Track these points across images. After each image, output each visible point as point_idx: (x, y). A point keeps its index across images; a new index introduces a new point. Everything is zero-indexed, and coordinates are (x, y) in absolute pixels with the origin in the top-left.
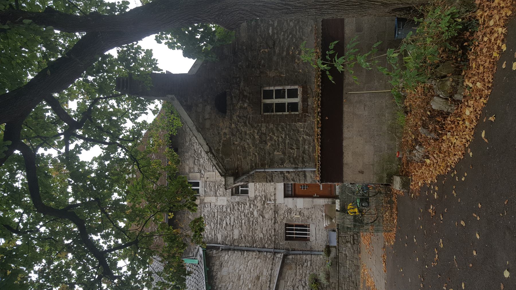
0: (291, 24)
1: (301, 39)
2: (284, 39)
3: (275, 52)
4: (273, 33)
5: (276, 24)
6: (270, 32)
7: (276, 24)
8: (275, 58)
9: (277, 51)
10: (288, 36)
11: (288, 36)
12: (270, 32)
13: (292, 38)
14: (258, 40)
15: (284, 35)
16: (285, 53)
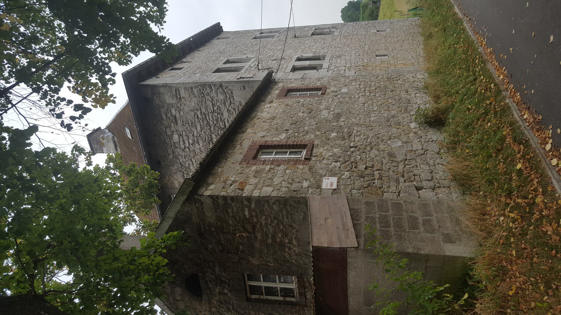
0: (275, 207)
2: (266, 224)
3: (256, 237)
5: (253, 206)
6: (247, 213)
7: (253, 206)
8: (257, 245)
9: (259, 236)
10: (272, 222)
11: (272, 222)
12: (247, 213)
14: (231, 222)
15: (266, 219)
16: (270, 241)
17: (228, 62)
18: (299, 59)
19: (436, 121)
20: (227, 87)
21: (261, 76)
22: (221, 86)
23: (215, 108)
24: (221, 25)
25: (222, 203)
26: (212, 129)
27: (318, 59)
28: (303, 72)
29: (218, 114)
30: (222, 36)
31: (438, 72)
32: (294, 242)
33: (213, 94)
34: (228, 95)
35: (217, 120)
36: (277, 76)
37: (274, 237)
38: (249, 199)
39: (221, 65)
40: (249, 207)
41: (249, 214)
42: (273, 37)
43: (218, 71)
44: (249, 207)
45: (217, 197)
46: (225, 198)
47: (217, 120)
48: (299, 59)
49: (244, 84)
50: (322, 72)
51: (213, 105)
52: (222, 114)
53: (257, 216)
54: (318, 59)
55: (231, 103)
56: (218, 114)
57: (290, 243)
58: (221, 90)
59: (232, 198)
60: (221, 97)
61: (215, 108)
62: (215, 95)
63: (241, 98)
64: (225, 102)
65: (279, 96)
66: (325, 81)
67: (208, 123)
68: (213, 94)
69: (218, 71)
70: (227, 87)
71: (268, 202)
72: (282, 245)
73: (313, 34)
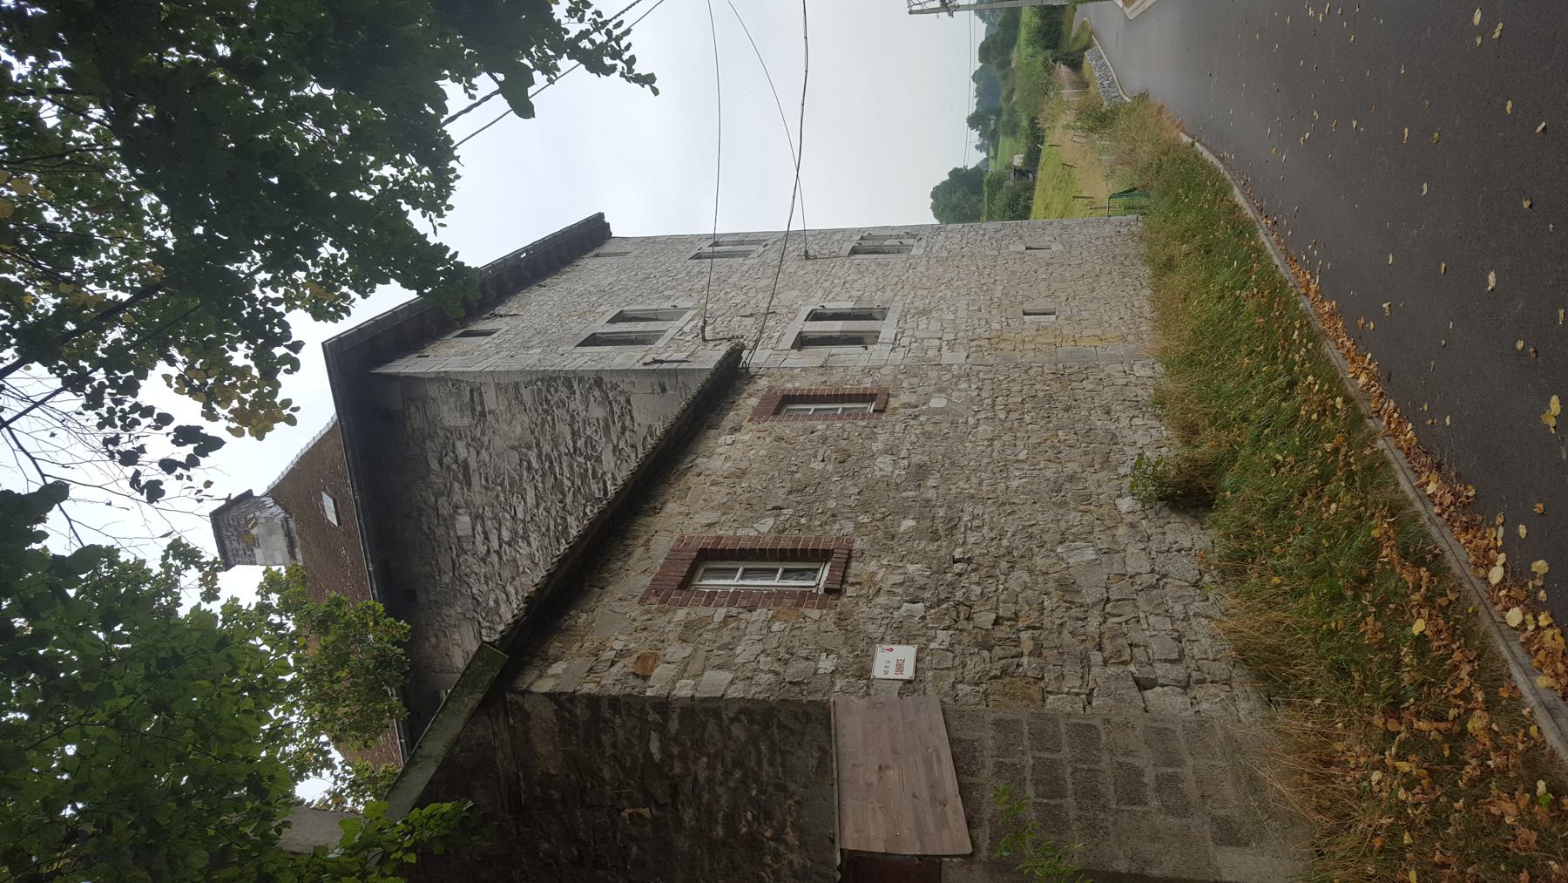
0: (737, 731)
1: (782, 788)
2: (710, 780)
3: (681, 821)
4: (667, 756)
5: (674, 725)
6: (654, 747)
7: (674, 725)
8: (682, 844)
9: (688, 816)
12: (654, 747)
13: (743, 781)
16: (720, 831)
17: (620, 317)
18: (815, 316)
19: (1187, 495)
20: (615, 387)
21: (711, 357)
22: (599, 382)
23: (580, 443)
24: (607, 220)
25: (586, 716)
26: (569, 500)
27: (867, 316)
28: (825, 350)
29: (588, 458)
30: (608, 248)
31: (1190, 361)
32: (791, 837)
33: (576, 404)
34: (616, 408)
35: (583, 476)
36: (756, 359)
37: (731, 821)
38: (663, 705)
39: (601, 326)
40: (662, 728)
41: (663, 749)
42: (745, 254)
43: (593, 340)
44: (662, 728)
45: (572, 697)
46: (593, 701)
47: (583, 476)
48: (815, 316)
49: (662, 377)
50: (878, 353)
51: (575, 435)
52: (598, 460)
53: (683, 757)
54: (867, 316)
55: (624, 429)
56: (588, 458)
57: (779, 838)
58: (597, 393)
59: (614, 702)
60: (598, 412)
61: (580, 443)
62: (581, 408)
63: (653, 416)
64: (607, 427)
65: (758, 414)
66: (885, 377)
67: (558, 485)
68: (576, 404)
69: (593, 340)
70: (615, 387)
71: (716, 714)
72: (754, 844)
73: (854, 251)
